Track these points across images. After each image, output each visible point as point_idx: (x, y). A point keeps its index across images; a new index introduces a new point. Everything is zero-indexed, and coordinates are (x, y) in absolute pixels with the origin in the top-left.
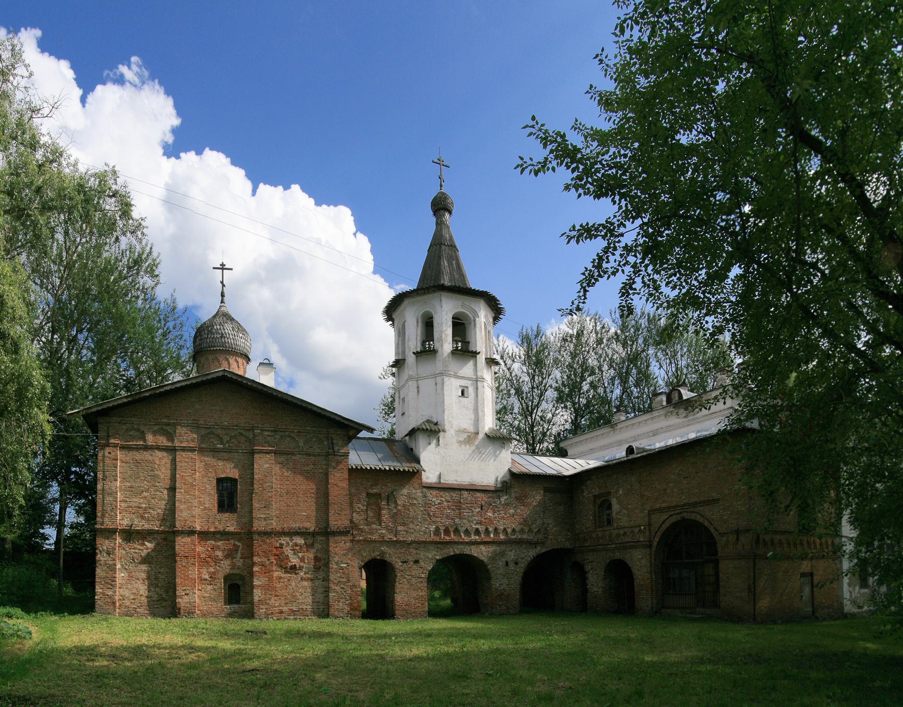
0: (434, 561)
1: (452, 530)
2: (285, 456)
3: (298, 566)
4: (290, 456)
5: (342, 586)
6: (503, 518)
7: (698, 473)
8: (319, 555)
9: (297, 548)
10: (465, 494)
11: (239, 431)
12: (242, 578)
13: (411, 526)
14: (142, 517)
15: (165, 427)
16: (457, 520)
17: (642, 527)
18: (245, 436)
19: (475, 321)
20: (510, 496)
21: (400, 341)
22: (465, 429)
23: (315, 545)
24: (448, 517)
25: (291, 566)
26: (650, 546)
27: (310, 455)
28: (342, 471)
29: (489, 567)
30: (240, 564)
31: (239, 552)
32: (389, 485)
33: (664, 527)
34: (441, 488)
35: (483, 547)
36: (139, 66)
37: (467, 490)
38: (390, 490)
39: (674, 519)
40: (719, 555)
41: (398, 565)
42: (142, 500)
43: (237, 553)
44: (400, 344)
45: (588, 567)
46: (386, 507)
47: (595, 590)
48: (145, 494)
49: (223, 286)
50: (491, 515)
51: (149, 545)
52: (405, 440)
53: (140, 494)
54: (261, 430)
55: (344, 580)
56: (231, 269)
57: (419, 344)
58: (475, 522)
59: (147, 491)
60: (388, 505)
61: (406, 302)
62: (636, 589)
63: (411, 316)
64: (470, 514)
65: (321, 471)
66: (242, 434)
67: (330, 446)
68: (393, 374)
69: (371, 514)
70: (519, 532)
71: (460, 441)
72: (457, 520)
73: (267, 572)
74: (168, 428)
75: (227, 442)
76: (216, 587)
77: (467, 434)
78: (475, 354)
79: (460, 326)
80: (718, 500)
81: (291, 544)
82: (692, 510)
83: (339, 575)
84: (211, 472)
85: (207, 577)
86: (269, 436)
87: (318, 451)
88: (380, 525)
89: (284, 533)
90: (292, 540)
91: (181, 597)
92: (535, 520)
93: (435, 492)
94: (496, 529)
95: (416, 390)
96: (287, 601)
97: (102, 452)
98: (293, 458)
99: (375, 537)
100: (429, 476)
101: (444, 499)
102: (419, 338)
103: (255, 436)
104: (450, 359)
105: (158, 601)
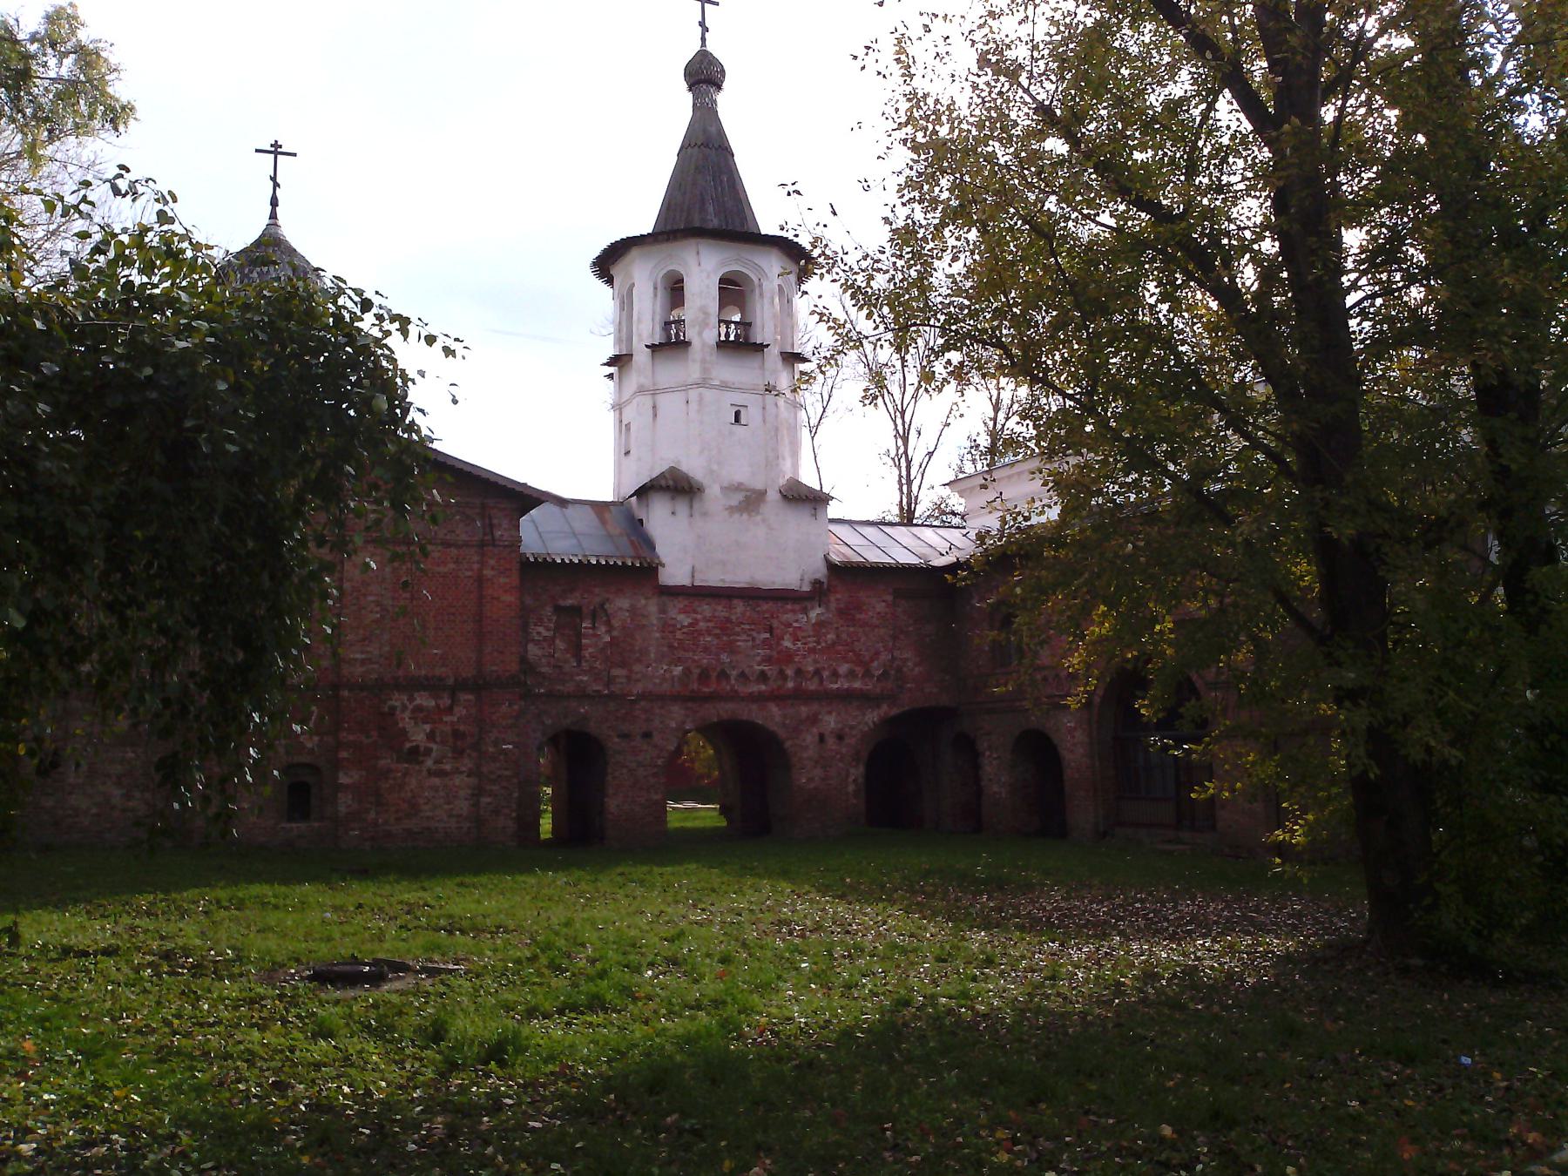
1: (714, 675)
3: (422, 749)
6: (812, 651)
8: (462, 728)
9: (421, 715)
10: (740, 607)
12: (314, 769)
13: (637, 668)
16: (724, 657)
19: (761, 286)
20: (827, 609)
21: (624, 317)
22: (740, 484)
23: (456, 709)
24: (706, 649)
25: (410, 749)
29: (788, 744)
32: (597, 590)
34: (695, 594)
35: (774, 709)
36: (670, 1057)
38: (597, 600)
46: (591, 631)
49: (276, 185)
52: (629, 503)
57: (658, 329)
58: (759, 658)
61: (635, 253)
63: (642, 274)
65: (469, 573)
67: (488, 530)
68: (610, 376)
70: (846, 676)
77: (744, 494)
79: (733, 290)
81: (411, 707)
87: (464, 537)
88: (579, 663)
89: (398, 686)
90: (411, 699)
92: (877, 653)
93: (681, 603)
94: (799, 672)
99: (570, 687)
100: (675, 572)
101: (699, 616)
102: (658, 318)
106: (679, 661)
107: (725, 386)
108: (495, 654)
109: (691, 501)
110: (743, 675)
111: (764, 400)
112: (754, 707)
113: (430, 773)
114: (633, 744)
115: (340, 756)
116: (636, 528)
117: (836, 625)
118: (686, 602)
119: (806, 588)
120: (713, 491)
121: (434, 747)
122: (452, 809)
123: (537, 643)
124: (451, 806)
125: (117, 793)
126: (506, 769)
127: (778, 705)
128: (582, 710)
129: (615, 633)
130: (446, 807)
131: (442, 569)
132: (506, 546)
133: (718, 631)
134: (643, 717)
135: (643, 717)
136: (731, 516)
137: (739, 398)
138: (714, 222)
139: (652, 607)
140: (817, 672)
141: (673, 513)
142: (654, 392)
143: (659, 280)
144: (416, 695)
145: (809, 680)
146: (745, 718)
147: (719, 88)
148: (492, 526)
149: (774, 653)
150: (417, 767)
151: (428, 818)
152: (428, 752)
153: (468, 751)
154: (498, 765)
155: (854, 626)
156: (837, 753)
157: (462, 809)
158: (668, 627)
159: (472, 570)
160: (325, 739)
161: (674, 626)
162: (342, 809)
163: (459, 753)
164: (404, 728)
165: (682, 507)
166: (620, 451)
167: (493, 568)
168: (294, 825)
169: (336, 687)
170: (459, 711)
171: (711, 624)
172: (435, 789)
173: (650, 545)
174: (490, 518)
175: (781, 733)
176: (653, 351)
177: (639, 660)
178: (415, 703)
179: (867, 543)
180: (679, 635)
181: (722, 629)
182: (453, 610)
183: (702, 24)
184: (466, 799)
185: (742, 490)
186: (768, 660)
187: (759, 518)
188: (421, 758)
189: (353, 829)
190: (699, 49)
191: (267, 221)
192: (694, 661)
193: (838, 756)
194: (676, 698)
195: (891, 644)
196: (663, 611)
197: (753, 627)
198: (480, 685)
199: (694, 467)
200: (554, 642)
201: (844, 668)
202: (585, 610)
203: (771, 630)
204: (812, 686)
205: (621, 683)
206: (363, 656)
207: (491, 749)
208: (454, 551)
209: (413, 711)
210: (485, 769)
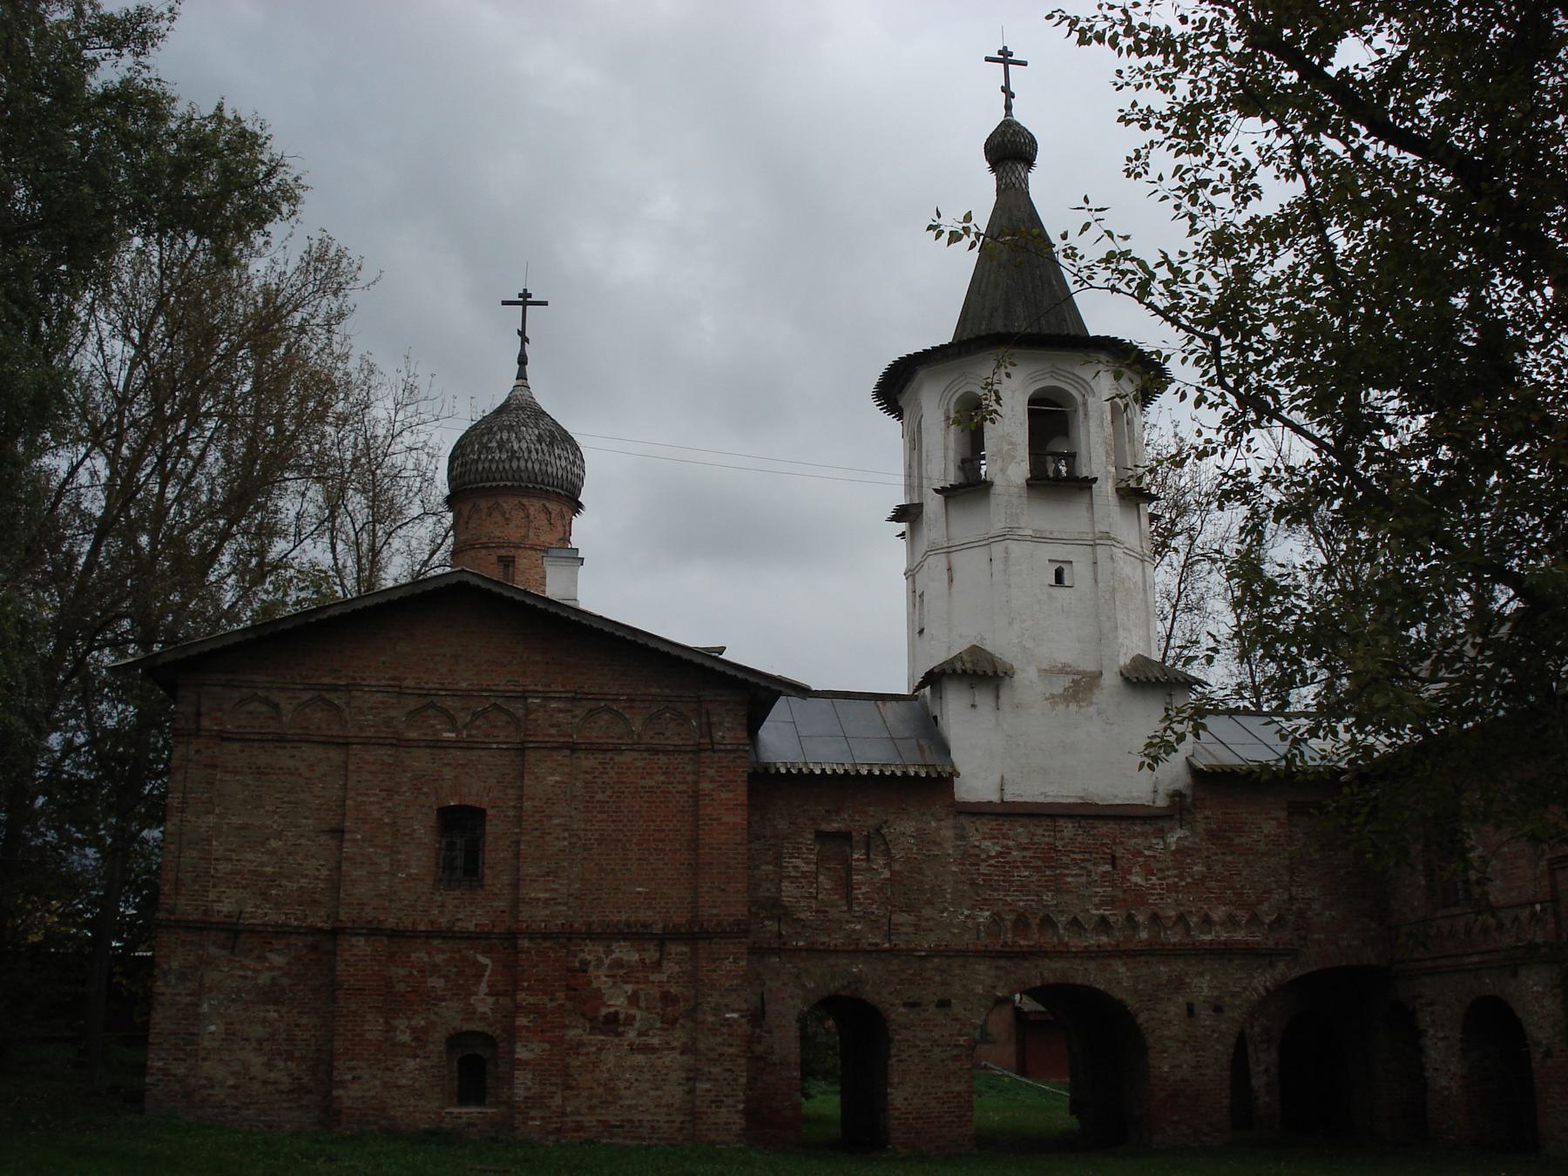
1: (1034, 922)
2: (600, 756)
3: (622, 1017)
4: (609, 755)
5: (728, 1065)
6: (1173, 888)
9: (621, 972)
10: (1068, 829)
11: (493, 700)
12: (489, 1040)
13: (928, 912)
14: (266, 897)
15: (327, 695)
16: (1047, 897)
17: (1538, 907)
18: (506, 712)
19: (1085, 404)
22: (1065, 665)
25: (607, 1016)
27: (657, 752)
29: (1141, 1019)
30: (485, 1009)
31: (485, 979)
32: (871, 811)
35: (1120, 968)
41: (898, 1014)
42: (265, 858)
43: (479, 982)
44: (915, 465)
46: (864, 864)
47: (1444, 1083)
48: (274, 844)
49: (525, 340)
50: (1139, 880)
51: (278, 960)
53: (263, 844)
54: (544, 698)
56: (545, 304)
58: (1096, 900)
59: (279, 835)
60: (868, 860)
61: (921, 374)
64: (1084, 879)
65: (682, 787)
69: (825, 882)
71: (1053, 696)
72: (1047, 897)
74: (332, 696)
75: (465, 726)
76: (426, 1063)
77: (1071, 677)
78: (1087, 484)
81: (607, 961)
83: (719, 1040)
84: (426, 794)
85: (406, 1038)
86: (560, 711)
88: (850, 909)
89: (591, 936)
90: (609, 952)
93: (986, 825)
94: (1155, 918)
95: (946, 577)
96: (595, 1101)
98: (618, 758)
99: (837, 940)
101: (1011, 843)
102: (951, 454)
103: (528, 711)
104: (1025, 500)
105: (291, 1091)
107: (1040, 538)
108: (716, 892)
109: (997, 689)
111: (1094, 553)
112: (1092, 966)
113: (633, 1049)
115: (517, 1023)
116: (930, 730)
117: (1206, 854)
118: (993, 824)
119: (1162, 802)
120: (1027, 677)
121: (639, 1014)
122: (659, 1097)
123: (793, 880)
124: (659, 1093)
125: (256, 1061)
126: (730, 1045)
127: (1125, 964)
128: (854, 970)
129: (896, 867)
130: (652, 1093)
134: (938, 978)
135: (938, 978)
136: (1053, 709)
137: (1060, 552)
138: (1021, 326)
140: (1181, 918)
141: (973, 706)
142: (949, 551)
143: (952, 404)
145: (1170, 929)
146: (1079, 981)
148: (710, 725)
149: (1120, 894)
150: (616, 1040)
151: (629, 1107)
152: (630, 1020)
153: (681, 1021)
154: (719, 1040)
155: (1232, 853)
156: (1213, 1031)
157: (673, 1096)
159: (687, 783)
160: (501, 1000)
161: (977, 856)
162: (520, 1092)
163: (670, 1023)
164: (599, 989)
165: (984, 699)
166: (913, 629)
167: (712, 781)
168: (464, 1110)
170: (670, 967)
171: (1029, 853)
173: (944, 749)
174: (708, 713)
175: (1132, 1003)
176: (947, 499)
177: (930, 903)
178: (614, 956)
179: (1215, 740)
180: (983, 869)
183: (1006, 89)
184: (680, 1084)
185: (1067, 673)
186: (1110, 901)
187: (1092, 709)
188: (620, 1029)
189: (533, 1118)
190: (1003, 119)
191: (514, 382)
192: (1006, 903)
193: (1216, 1035)
194: (983, 954)
195: (1286, 878)
196: (962, 837)
197: (1087, 856)
198: (694, 935)
199: (1002, 644)
200: (817, 879)
201: (1218, 914)
202: (856, 837)
203: (1113, 861)
204: (1174, 937)
205: (907, 934)
206: (547, 895)
207: (711, 1019)
208: (663, 758)
209: (610, 967)
210: (701, 1045)
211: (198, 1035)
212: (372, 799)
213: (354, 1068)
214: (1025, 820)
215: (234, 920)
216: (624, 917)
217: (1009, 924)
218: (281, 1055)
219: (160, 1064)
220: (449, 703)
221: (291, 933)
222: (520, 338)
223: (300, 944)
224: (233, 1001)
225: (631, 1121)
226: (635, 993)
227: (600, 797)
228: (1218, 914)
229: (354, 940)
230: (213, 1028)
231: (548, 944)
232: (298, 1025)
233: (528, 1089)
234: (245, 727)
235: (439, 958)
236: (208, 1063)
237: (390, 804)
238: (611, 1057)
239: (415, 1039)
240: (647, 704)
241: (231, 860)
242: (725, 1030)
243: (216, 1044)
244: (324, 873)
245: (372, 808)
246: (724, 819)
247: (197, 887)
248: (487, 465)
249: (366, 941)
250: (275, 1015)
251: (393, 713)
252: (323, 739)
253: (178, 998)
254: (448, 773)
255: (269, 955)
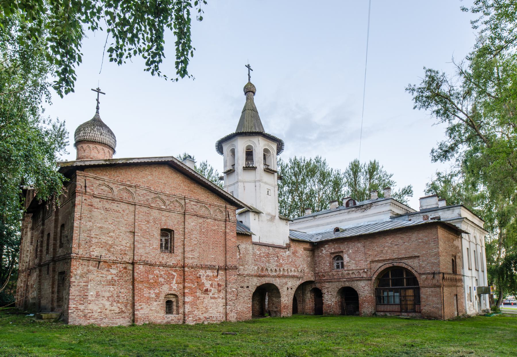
0: (256, 287)
2: (202, 219)
3: (209, 290)
4: (205, 219)
5: (233, 302)
6: (287, 263)
7: (404, 243)
8: (220, 283)
9: (209, 278)
11: (176, 199)
13: (246, 266)
17: (366, 270)
22: (269, 213)
26: (371, 280)
28: (233, 231)
31: (175, 279)
33: (380, 270)
37: (272, 247)
39: (387, 266)
40: (420, 285)
42: (109, 238)
43: (173, 280)
45: (324, 291)
49: (98, 103)
53: (108, 234)
55: (234, 298)
62: (360, 302)
65: (221, 230)
66: (177, 201)
73: (193, 292)
80: (418, 257)
81: (205, 275)
82: (400, 261)
86: (194, 205)
89: (202, 267)
90: (206, 272)
91: (138, 310)
94: (284, 269)
95: (243, 188)
96: (203, 312)
97: (459, 182)
98: (207, 221)
105: (119, 313)
106: (256, 265)
108: (230, 258)
110: (271, 270)
112: (273, 279)
114: (244, 290)
119: (285, 245)
121: (212, 289)
125: (107, 304)
131: (214, 228)
132: (232, 222)
133: (266, 256)
139: (250, 247)
142: (255, 182)
144: (207, 271)
147: (254, 93)
150: (207, 296)
154: (231, 296)
158: (254, 254)
163: (219, 291)
169: (184, 267)
171: (264, 254)
172: (212, 303)
178: (207, 274)
181: (267, 256)
182: (217, 243)
186: (277, 266)
187: (274, 224)
188: (208, 293)
191: (95, 114)
194: (256, 276)
196: (253, 249)
201: (293, 269)
204: (286, 274)
207: (230, 290)
208: (217, 222)
211: (87, 296)
212: (143, 223)
213: (141, 305)
214: (264, 247)
215: (99, 258)
216: (209, 263)
217: (260, 270)
218: (115, 301)
219: (74, 306)
220: (164, 197)
221: (118, 263)
222: (97, 102)
223: (121, 267)
224: (99, 284)
225: (211, 317)
226: (212, 284)
227: (203, 230)
228: (293, 269)
229: (140, 266)
230: (92, 293)
231: (193, 270)
232: (120, 292)
233: (189, 309)
234: (101, 194)
235: (162, 273)
236: (91, 305)
237: (148, 225)
238: (206, 300)
239: (156, 296)
240: (214, 207)
241: (97, 238)
242: (232, 293)
243: (93, 299)
244: (128, 245)
245: (143, 226)
246: (232, 240)
247: (86, 246)
248: (93, 135)
249: (143, 267)
250: (113, 289)
251: (149, 197)
252: (127, 202)
253: (80, 283)
254: (163, 218)
255: (110, 270)
